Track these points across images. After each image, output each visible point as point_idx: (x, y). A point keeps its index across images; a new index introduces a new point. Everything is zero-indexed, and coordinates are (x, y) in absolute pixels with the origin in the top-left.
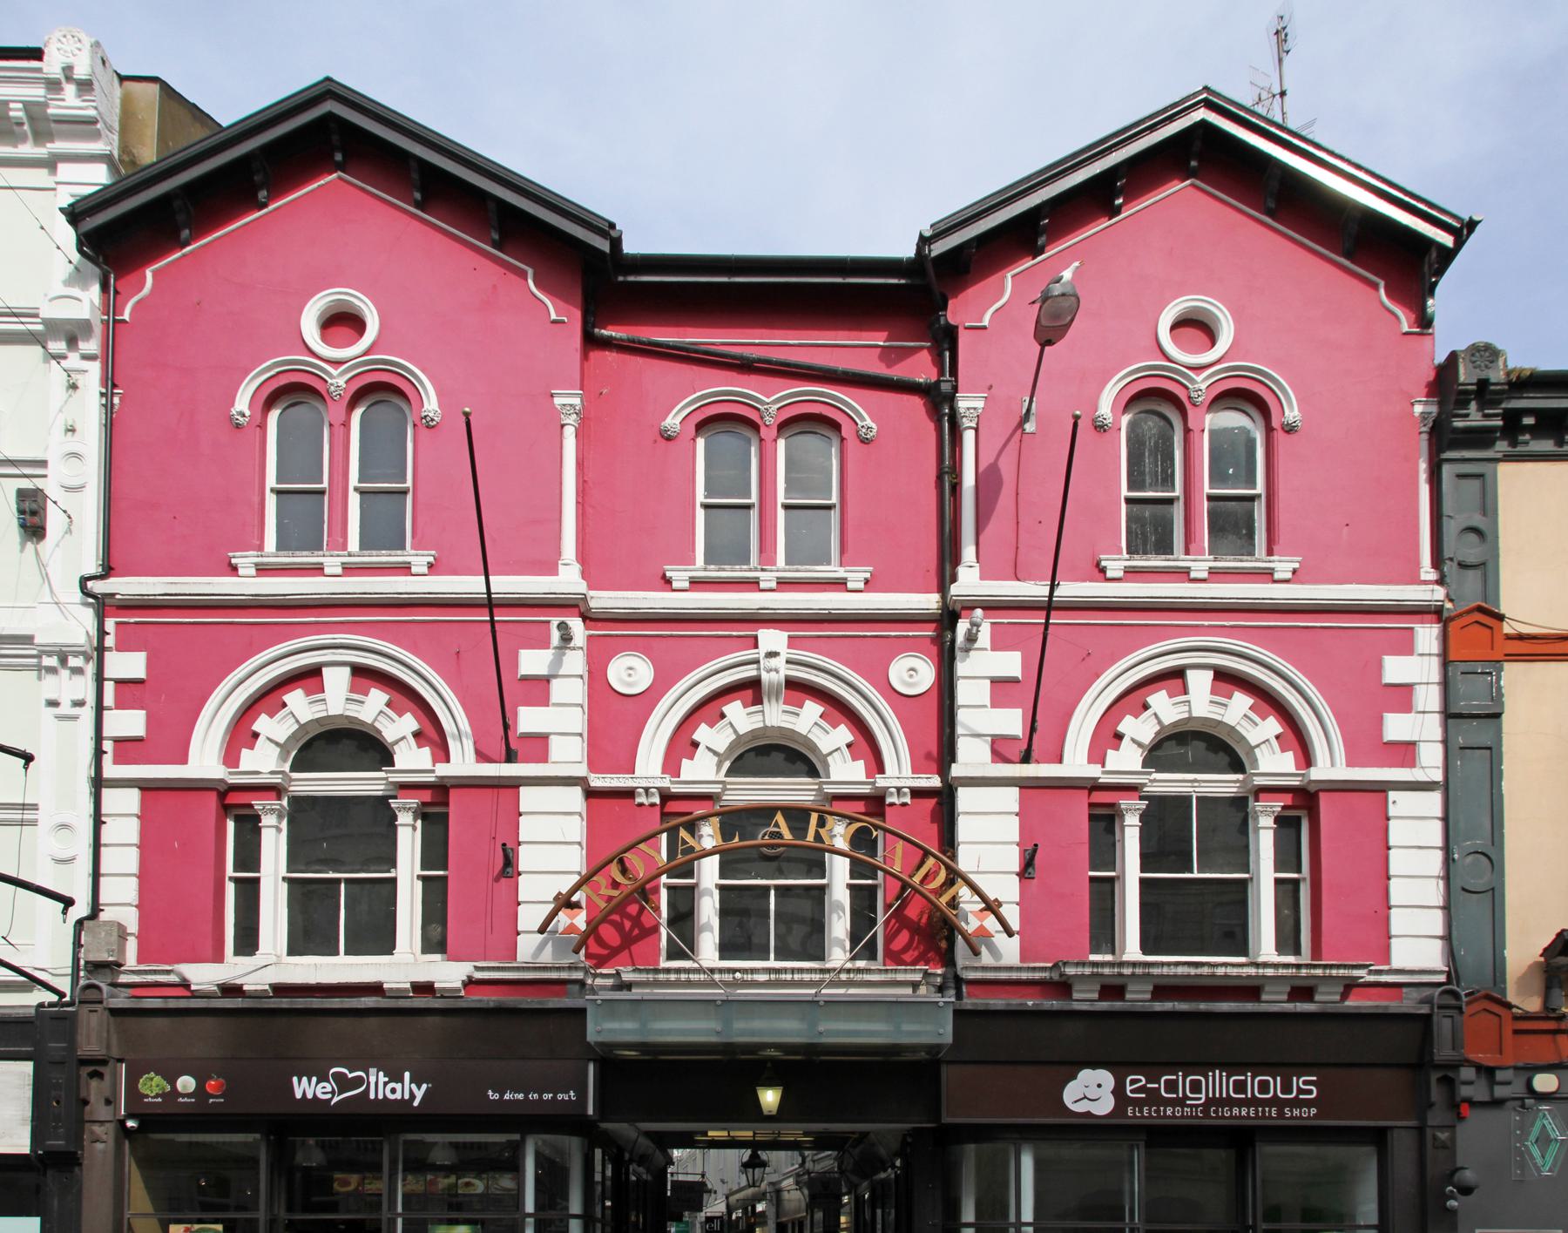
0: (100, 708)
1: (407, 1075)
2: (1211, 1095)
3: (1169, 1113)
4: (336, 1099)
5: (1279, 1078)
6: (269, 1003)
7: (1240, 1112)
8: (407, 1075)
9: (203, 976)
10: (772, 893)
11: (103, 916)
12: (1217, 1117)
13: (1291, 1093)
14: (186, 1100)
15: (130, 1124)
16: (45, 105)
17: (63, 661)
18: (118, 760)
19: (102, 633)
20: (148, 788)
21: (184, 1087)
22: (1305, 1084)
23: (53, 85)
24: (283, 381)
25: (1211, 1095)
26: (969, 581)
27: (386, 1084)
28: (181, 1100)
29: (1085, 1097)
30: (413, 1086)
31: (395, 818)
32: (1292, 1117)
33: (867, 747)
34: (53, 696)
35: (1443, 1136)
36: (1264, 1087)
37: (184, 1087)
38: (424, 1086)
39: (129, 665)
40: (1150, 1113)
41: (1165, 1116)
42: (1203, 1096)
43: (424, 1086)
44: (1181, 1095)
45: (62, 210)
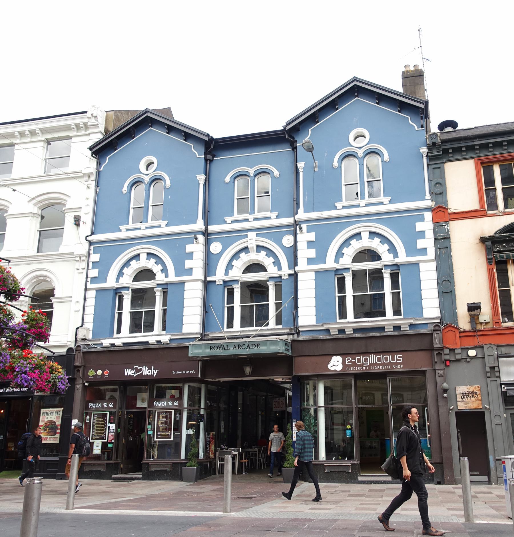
0: (88, 270)
1: (153, 367)
2: (371, 363)
3: (359, 369)
4: (135, 375)
5: (391, 356)
6: (120, 348)
7: (380, 368)
8: (153, 367)
9: (106, 342)
10: (255, 306)
11: (84, 326)
12: (373, 370)
13: (395, 360)
14: (99, 377)
15: (86, 384)
16: (87, 123)
17: (80, 258)
18: (92, 283)
19: (90, 250)
20: (98, 291)
21: (99, 373)
22: (399, 357)
23: (89, 118)
24: (133, 182)
25: (371, 363)
26: (301, 215)
27: (147, 370)
28: (98, 377)
29: (334, 365)
30: (154, 370)
31: (155, 293)
32: (395, 369)
33: (277, 263)
34: (78, 268)
35: (441, 372)
36: (386, 359)
37: (99, 373)
38: (157, 371)
39: (95, 257)
40: (353, 369)
41: (358, 370)
42: (368, 363)
43: (157, 371)
44: (362, 363)
45: (88, 148)
